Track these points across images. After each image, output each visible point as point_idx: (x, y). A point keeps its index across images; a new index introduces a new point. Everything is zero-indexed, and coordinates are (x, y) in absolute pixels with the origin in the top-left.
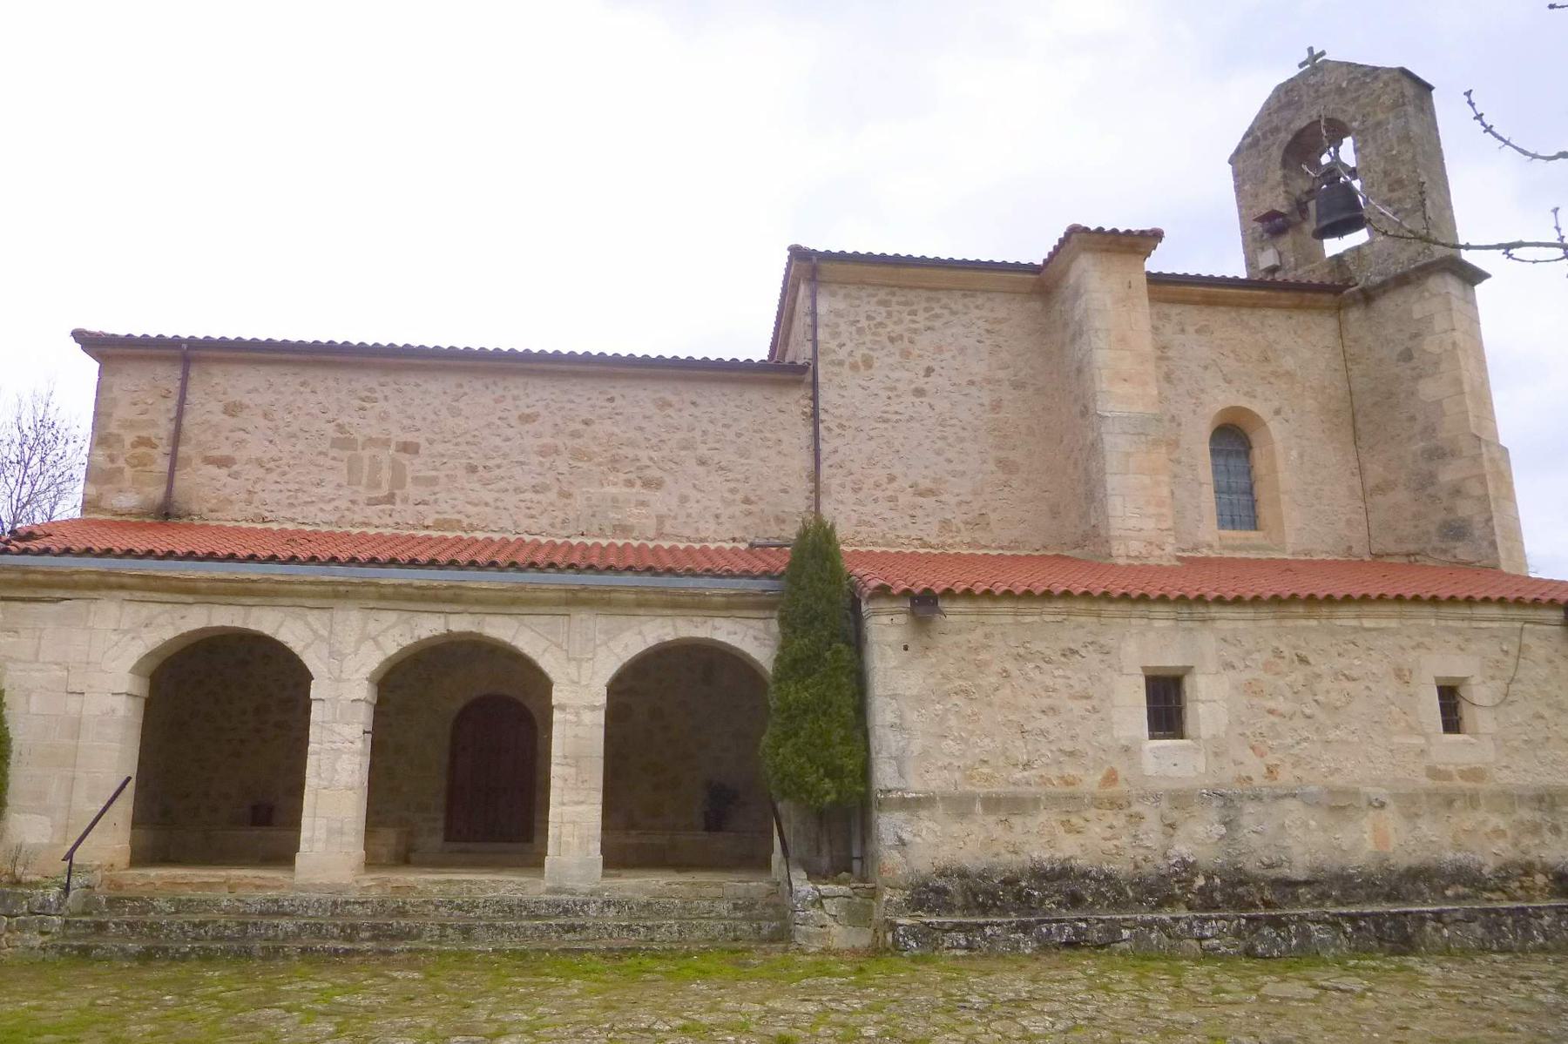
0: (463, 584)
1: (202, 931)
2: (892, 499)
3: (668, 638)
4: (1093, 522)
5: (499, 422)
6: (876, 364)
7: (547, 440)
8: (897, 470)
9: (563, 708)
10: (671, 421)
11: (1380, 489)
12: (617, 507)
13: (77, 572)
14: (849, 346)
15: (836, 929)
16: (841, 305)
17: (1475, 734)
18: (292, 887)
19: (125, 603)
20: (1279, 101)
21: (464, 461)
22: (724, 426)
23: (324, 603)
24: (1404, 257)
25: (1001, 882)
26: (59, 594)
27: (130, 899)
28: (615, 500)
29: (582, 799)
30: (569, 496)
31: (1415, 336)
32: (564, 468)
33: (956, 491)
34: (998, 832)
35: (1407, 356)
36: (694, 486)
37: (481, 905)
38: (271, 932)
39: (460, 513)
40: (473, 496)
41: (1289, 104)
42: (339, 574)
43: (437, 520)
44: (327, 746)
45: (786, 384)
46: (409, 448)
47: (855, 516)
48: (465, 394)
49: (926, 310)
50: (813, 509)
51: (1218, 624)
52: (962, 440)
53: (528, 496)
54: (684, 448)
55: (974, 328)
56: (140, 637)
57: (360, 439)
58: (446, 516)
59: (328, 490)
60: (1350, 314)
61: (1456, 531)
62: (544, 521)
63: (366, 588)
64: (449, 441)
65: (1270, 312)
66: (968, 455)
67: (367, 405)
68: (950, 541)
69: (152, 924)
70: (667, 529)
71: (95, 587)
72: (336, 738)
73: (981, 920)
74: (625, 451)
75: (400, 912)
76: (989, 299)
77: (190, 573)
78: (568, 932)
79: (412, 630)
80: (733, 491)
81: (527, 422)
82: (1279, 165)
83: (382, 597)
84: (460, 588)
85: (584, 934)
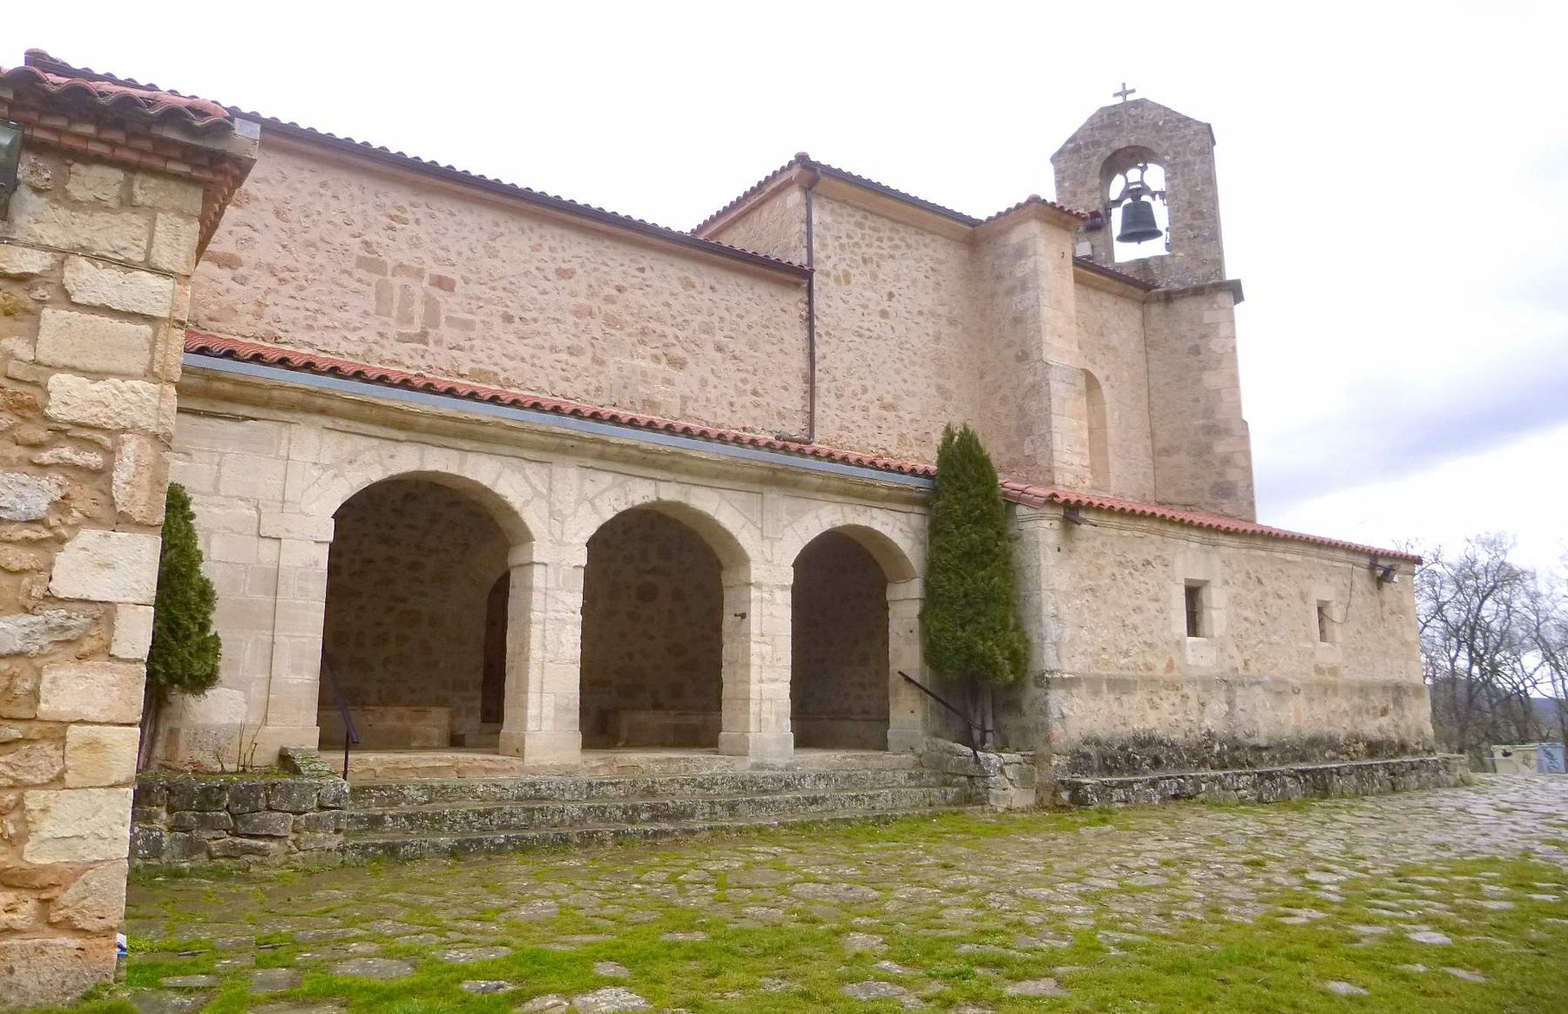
0: (685, 452)
1: (487, 820)
2: (865, 409)
3: (839, 524)
4: (1027, 452)
5: (535, 272)
6: (853, 281)
7: (582, 300)
8: (869, 383)
9: (759, 586)
10: (693, 302)
11: (1168, 451)
12: (646, 382)
13: (281, 387)
14: (834, 259)
15: (1012, 791)
16: (828, 220)
17: (1333, 642)
18: (522, 770)
19: (325, 431)
20: (1102, 120)
21: (501, 309)
22: (738, 316)
23: (544, 457)
24: (1200, 273)
25: (1119, 748)
26: (244, 411)
27: (377, 789)
28: (644, 374)
29: (777, 676)
30: (601, 363)
31: (1203, 337)
32: (598, 334)
33: (910, 409)
34: (1115, 707)
35: (1196, 351)
36: (712, 370)
37: (719, 782)
38: (557, 819)
39: (496, 364)
40: (510, 350)
41: (1111, 126)
42: (571, 426)
43: (472, 369)
44: (551, 614)
45: (787, 284)
46: (441, 283)
47: (837, 421)
48: (502, 234)
49: (890, 239)
50: (808, 409)
51: (1222, 549)
52: (913, 363)
53: (564, 356)
54: (705, 332)
55: (922, 264)
56: (343, 476)
57: (391, 264)
58: (481, 366)
59: (352, 316)
60: (1152, 309)
61: (1224, 490)
62: (579, 386)
63: (592, 445)
64: (485, 284)
65: (1105, 296)
66: (918, 377)
67: (398, 226)
68: (905, 454)
69: (434, 815)
70: (689, 411)
71: (290, 407)
72: (560, 606)
73: (1132, 779)
74: (653, 325)
75: (649, 792)
76: (933, 240)
77: (414, 405)
78: (811, 804)
79: (626, 495)
80: (744, 381)
81: (564, 277)
82: (1098, 174)
83: (601, 456)
84: (681, 454)
85: (825, 806)
